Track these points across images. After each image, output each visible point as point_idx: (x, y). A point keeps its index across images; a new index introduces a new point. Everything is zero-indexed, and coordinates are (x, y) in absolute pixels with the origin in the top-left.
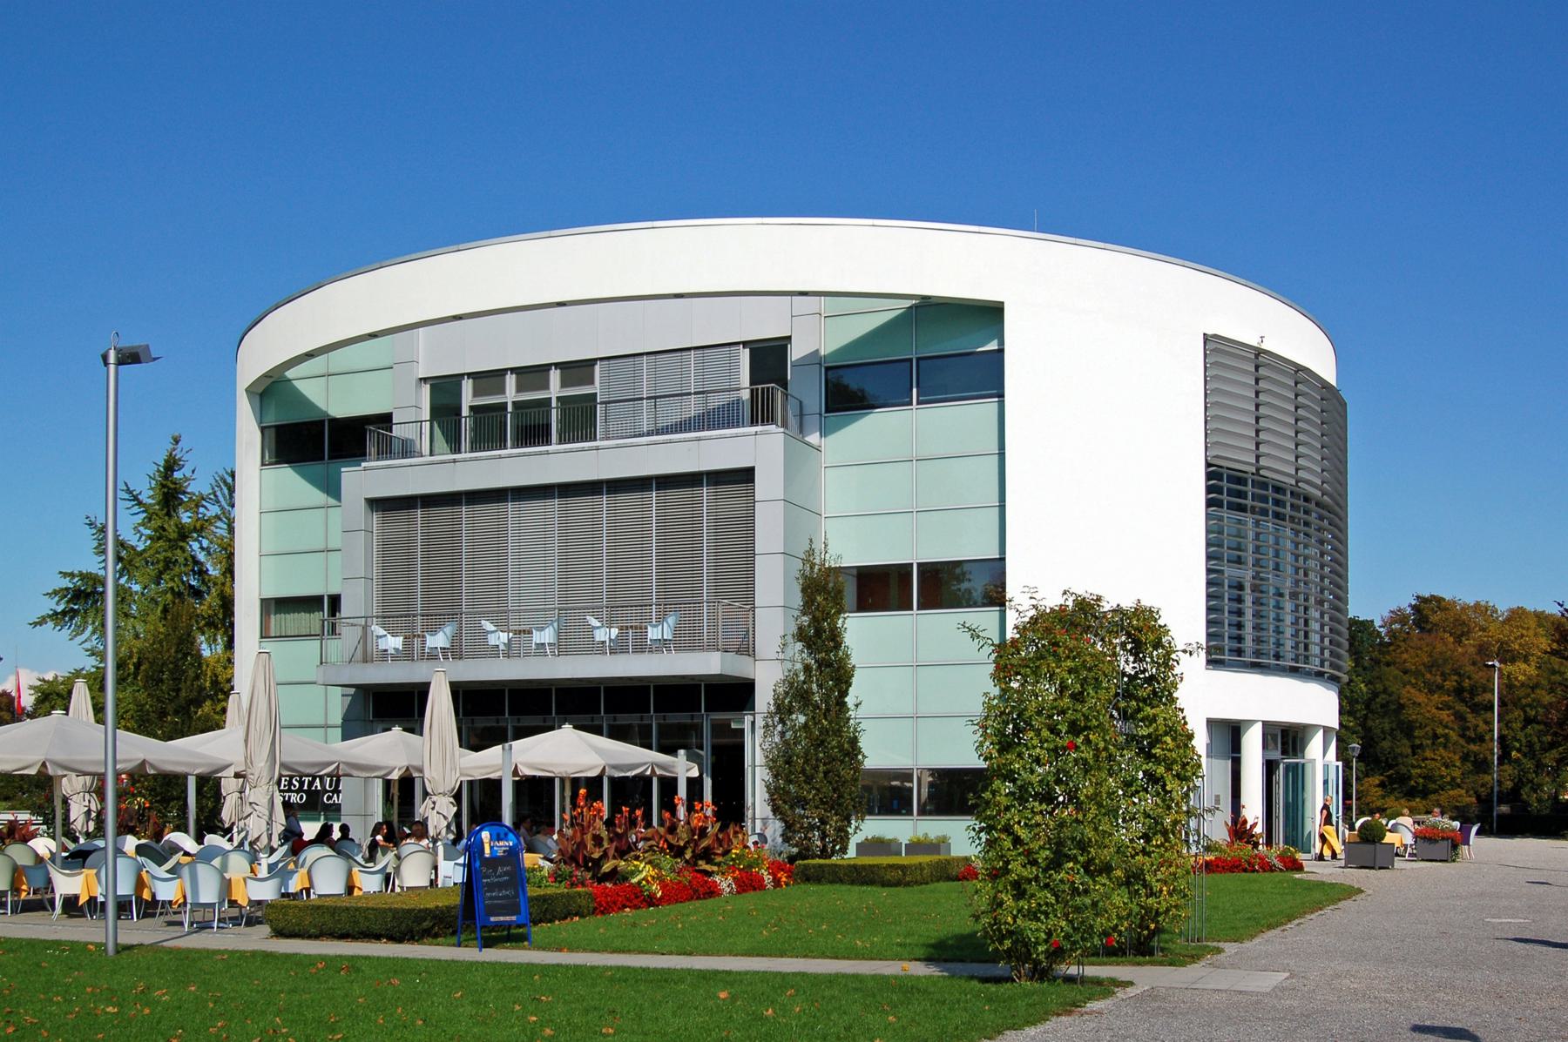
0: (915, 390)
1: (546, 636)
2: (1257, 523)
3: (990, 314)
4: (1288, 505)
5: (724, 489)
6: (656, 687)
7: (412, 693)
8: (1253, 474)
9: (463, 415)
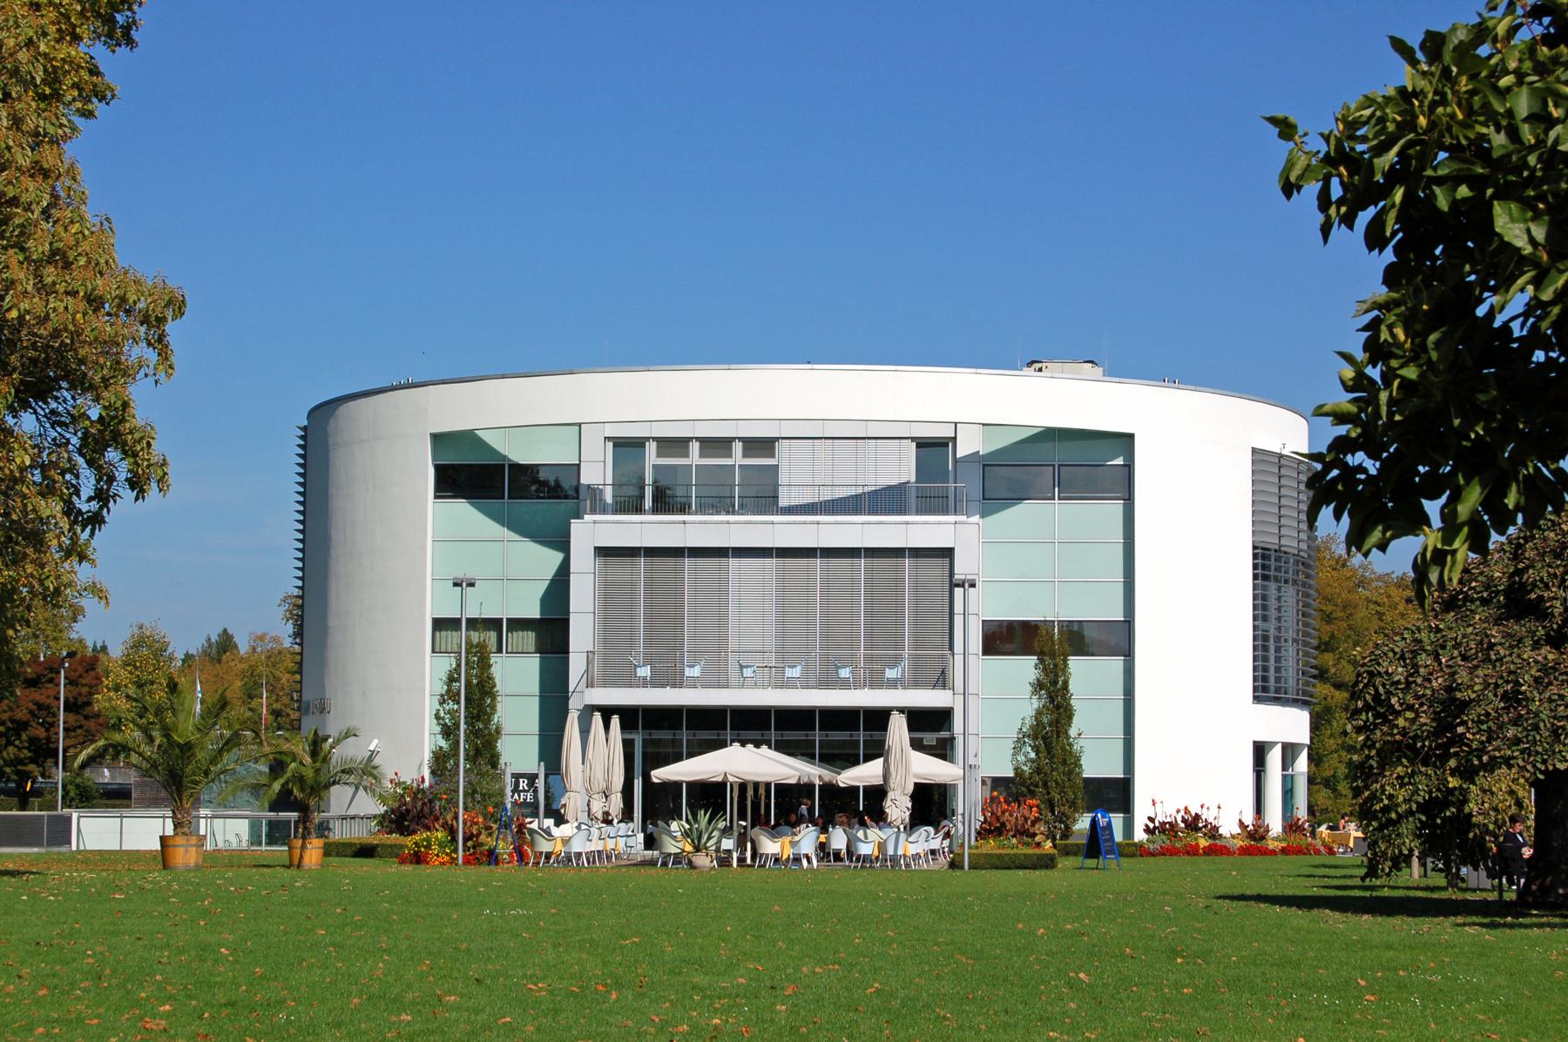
0: (1057, 489)
1: (644, 672)
2: (1279, 589)
3: (1125, 441)
4: (1273, 568)
5: (922, 561)
6: (864, 711)
7: (770, 711)
8: (1276, 551)
9: (647, 483)
